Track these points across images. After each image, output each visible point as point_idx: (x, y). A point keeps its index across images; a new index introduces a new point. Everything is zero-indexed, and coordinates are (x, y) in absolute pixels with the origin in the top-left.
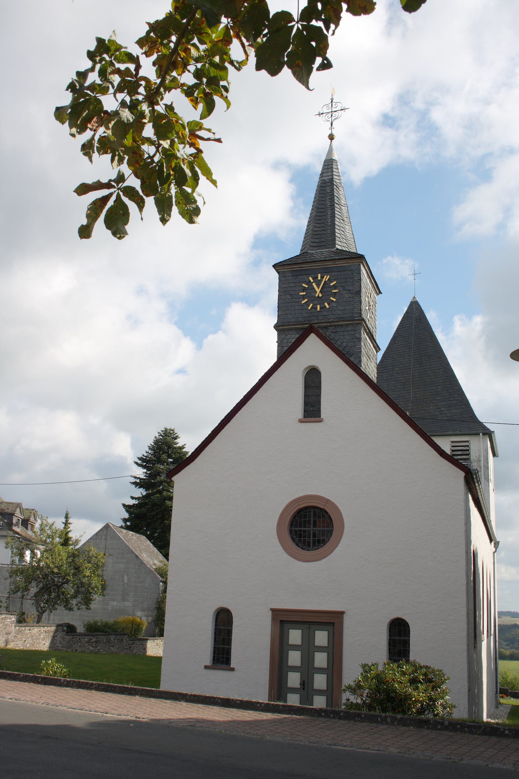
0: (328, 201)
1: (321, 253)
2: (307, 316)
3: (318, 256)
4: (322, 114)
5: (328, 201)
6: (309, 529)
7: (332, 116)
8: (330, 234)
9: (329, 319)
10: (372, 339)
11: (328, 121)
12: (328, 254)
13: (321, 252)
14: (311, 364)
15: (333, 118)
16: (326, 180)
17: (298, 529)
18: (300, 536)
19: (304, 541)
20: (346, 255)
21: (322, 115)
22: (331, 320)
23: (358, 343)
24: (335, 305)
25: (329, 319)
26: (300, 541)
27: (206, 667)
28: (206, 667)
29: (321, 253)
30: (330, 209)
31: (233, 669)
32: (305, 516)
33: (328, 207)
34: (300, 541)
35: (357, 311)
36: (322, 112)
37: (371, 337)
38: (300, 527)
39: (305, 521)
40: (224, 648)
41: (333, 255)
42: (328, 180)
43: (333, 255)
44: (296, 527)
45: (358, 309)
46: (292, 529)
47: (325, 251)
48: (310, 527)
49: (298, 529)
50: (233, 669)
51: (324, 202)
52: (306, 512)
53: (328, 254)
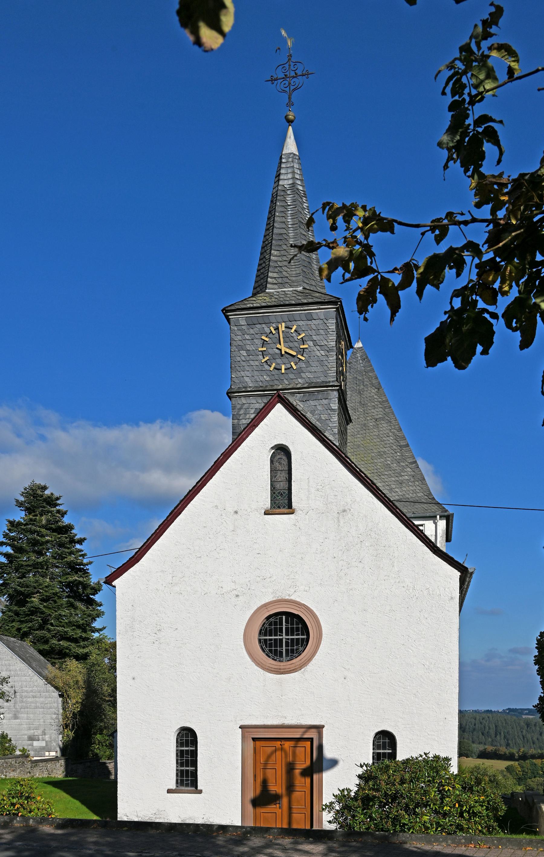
0: (290, 217)
1: (283, 293)
2: (267, 379)
3: (281, 298)
4: (276, 80)
5: (290, 217)
6: (281, 637)
7: (290, 83)
8: (294, 267)
9: (297, 384)
10: (345, 410)
11: (285, 91)
12: (294, 295)
13: (284, 291)
14: (278, 443)
15: (292, 88)
16: (285, 186)
17: (268, 638)
18: (271, 645)
19: (276, 651)
20: (317, 297)
21: (276, 82)
22: (299, 386)
23: (333, 415)
24: (304, 366)
25: (297, 384)
26: (271, 651)
27: (169, 791)
28: (169, 791)
29: (283, 293)
30: (292, 229)
31: (200, 792)
32: (276, 624)
33: (290, 226)
34: (271, 651)
35: (332, 374)
36: (275, 77)
37: (345, 408)
38: (270, 635)
39: (276, 629)
40: (189, 770)
41: (300, 298)
42: (288, 186)
43: (300, 298)
44: (265, 635)
45: (333, 372)
46: (261, 638)
47: (289, 291)
48: (282, 635)
49: (268, 638)
50: (200, 792)
51: (284, 219)
52: (277, 619)
53: (294, 295)
